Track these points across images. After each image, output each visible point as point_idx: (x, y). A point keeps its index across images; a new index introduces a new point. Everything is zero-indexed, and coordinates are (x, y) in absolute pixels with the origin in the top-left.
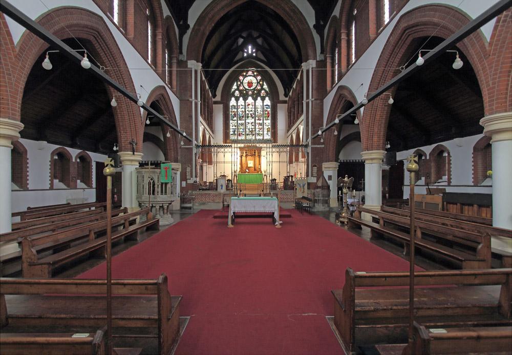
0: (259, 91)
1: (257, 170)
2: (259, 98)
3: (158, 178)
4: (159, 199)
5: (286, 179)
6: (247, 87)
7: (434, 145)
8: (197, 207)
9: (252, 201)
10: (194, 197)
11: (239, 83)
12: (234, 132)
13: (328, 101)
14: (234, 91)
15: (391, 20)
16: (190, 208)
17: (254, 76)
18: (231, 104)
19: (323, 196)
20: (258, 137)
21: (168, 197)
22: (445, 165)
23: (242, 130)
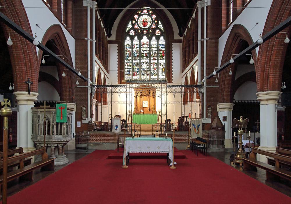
0: (154, 30)
1: (151, 110)
2: (154, 38)
3: (54, 118)
4: (54, 139)
5: (181, 120)
6: (142, 26)
8: (92, 147)
11: (134, 22)
12: (129, 71)
14: (129, 31)
16: (85, 148)
17: (149, 15)
18: (126, 44)
23: (137, 70)
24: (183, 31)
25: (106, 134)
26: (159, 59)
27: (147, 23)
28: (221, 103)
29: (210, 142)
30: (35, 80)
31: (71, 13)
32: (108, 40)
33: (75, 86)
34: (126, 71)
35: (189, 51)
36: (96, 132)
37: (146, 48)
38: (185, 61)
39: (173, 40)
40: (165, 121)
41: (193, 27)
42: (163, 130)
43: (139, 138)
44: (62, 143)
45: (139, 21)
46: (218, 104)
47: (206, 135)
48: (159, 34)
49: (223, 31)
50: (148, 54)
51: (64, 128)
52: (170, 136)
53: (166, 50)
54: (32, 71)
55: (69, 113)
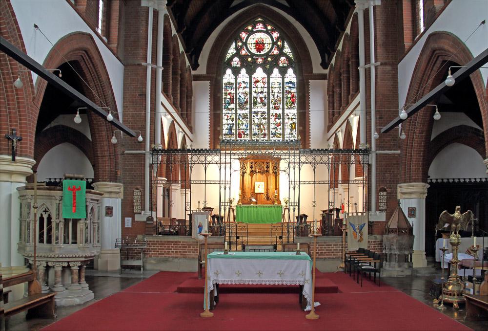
0: (276, 58)
1: (271, 198)
2: (276, 71)
3: (58, 209)
4: (57, 253)
5: (327, 215)
6: (254, 51)
8: (153, 266)
9: (254, 261)
10: (146, 247)
11: (240, 44)
12: (231, 129)
14: (231, 59)
16: (138, 268)
17: (267, 32)
18: (225, 81)
19: (400, 248)
21: (79, 248)
23: (244, 127)
25: (180, 242)
26: (286, 107)
27: (264, 46)
28: (405, 182)
29: (381, 258)
30: (26, 132)
31: (118, 18)
32: (193, 75)
33: (122, 151)
34: (225, 129)
35: (341, 94)
36: (162, 238)
37: (262, 87)
39: (310, 75)
40: (297, 217)
41: (346, 50)
42: (291, 234)
44: (77, 261)
45: (248, 42)
46: (399, 185)
47: (377, 244)
48: (286, 65)
49: (406, 50)
50: (265, 98)
51: (82, 231)
52: (307, 247)
53: (298, 92)
54: (20, 115)
55: (92, 199)
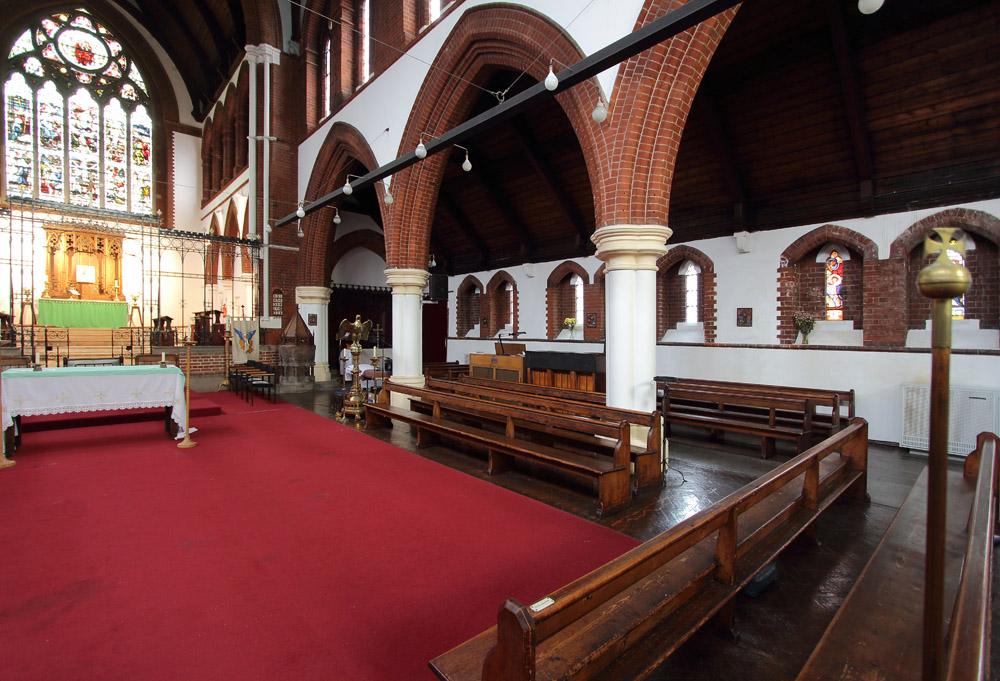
5: (202, 320)
7: (494, 272)
13: (309, 152)
15: (445, 15)
20: (111, 206)
22: (508, 307)
23: (53, 176)
24: (204, 108)
38: (210, 180)
41: (231, 107)
43: (63, 369)
52: (175, 359)
